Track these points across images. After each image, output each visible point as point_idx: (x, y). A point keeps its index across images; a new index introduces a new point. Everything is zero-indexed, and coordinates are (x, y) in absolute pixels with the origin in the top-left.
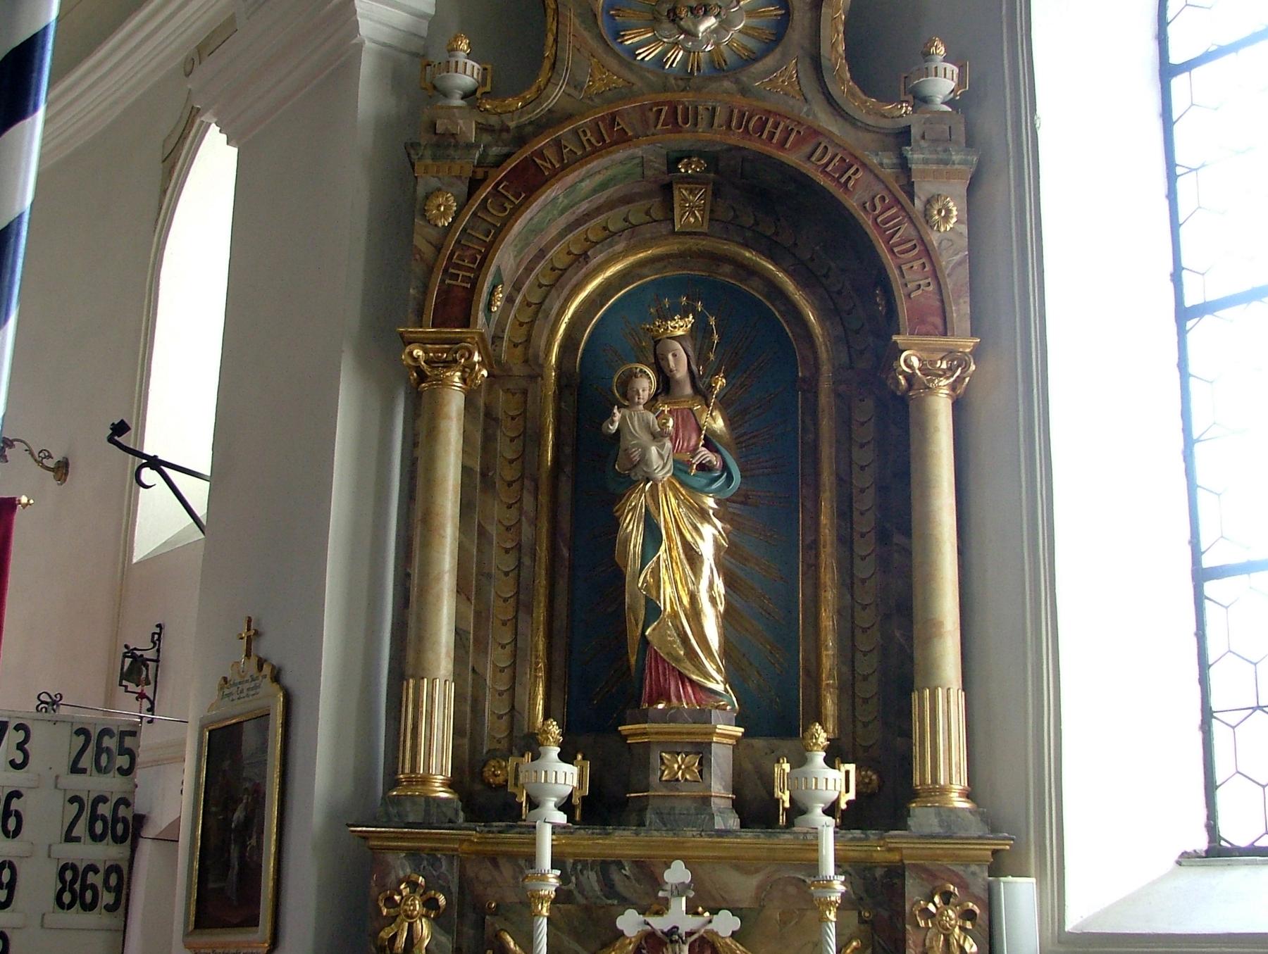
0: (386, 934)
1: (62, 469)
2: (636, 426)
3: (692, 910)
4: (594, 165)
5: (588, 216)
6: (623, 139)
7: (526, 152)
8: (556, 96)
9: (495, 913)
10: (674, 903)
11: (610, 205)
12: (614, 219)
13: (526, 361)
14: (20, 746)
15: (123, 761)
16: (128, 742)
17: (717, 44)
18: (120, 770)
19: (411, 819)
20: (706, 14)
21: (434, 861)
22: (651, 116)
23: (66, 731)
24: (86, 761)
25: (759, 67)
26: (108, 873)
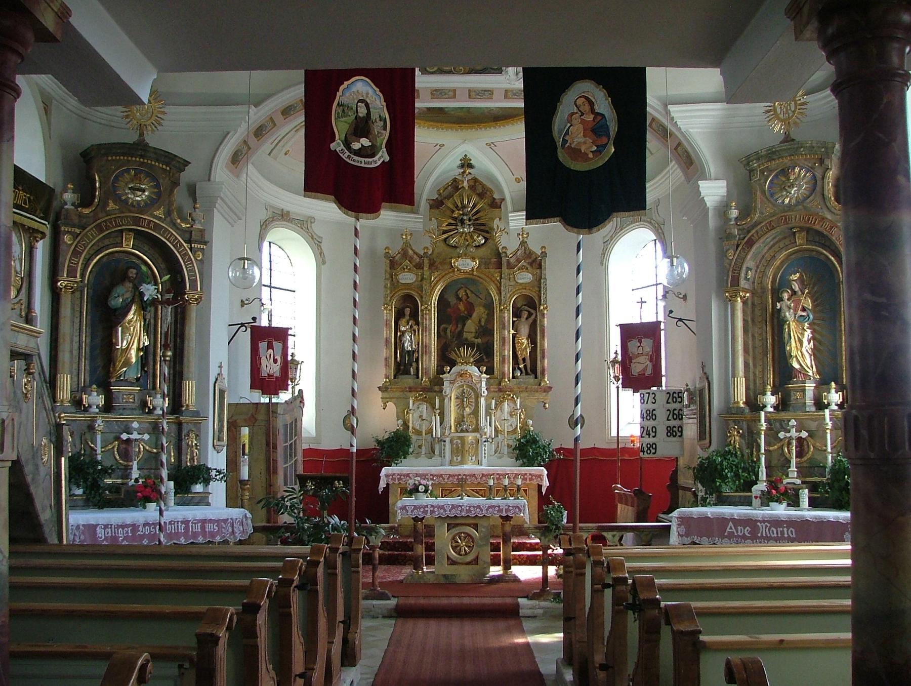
0: (728, 440)
1: (685, 298)
2: (784, 308)
3: (796, 431)
4: (767, 236)
5: (774, 245)
6: (773, 228)
7: (750, 234)
8: (756, 217)
9: (755, 434)
10: (791, 430)
11: (780, 241)
12: (782, 245)
13: (761, 289)
14: (654, 398)
15: (679, 400)
16: (680, 395)
17: (798, 195)
18: (679, 402)
19: (733, 412)
20: (793, 187)
21: (739, 422)
22: (780, 220)
23: (665, 394)
24: (670, 400)
25: (808, 200)
26: (678, 428)
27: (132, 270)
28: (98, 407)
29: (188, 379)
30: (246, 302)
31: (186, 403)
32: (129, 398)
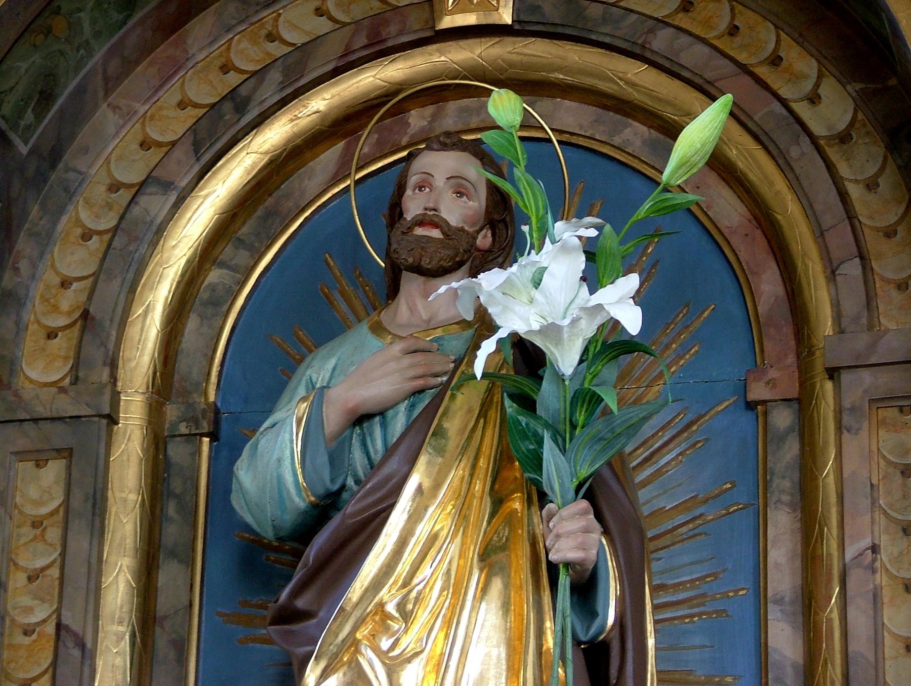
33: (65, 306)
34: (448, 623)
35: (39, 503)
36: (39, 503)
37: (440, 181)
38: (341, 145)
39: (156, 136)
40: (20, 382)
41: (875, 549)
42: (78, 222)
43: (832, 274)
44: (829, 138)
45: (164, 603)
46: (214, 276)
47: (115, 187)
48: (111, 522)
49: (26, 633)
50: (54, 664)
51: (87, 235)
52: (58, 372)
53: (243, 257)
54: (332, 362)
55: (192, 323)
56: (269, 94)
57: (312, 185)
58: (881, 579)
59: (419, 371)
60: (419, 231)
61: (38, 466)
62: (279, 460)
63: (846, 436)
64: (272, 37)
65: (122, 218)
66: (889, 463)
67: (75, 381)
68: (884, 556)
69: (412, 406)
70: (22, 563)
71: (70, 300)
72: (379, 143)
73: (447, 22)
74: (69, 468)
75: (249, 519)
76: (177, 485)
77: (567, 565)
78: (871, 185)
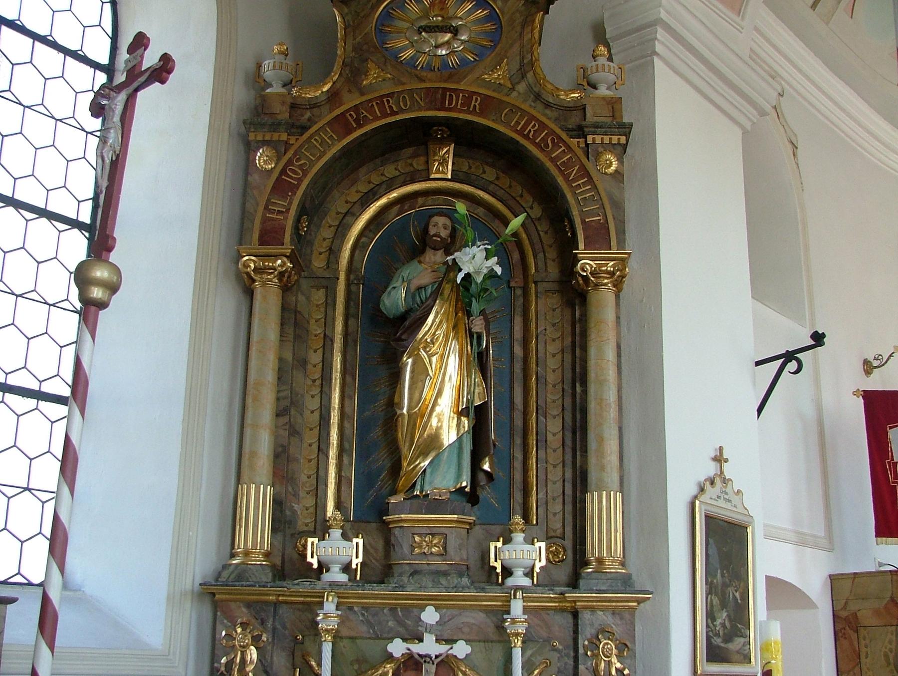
27: (436, 219)
28: (346, 568)
29: (600, 490)
30: (876, 363)
31: (593, 555)
32: (430, 545)
33: (324, 246)
34: (444, 346)
35: (318, 300)
36: (318, 300)
37: (440, 225)
38: (399, 206)
39: (349, 199)
40: (312, 267)
41: (545, 329)
42: (328, 223)
43: (535, 257)
44: (536, 219)
45: (350, 330)
46: (363, 239)
47: (338, 213)
48: (337, 306)
49: (316, 336)
50: (324, 345)
51: (330, 227)
52: (324, 264)
53: (371, 235)
54: (408, 271)
55: (357, 252)
56: (382, 190)
57: (391, 216)
58: (547, 337)
59: (435, 277)
60: (434, 238)
61: (317, 290)
62: (398, 299)
63: (539, 299)
64: (382, 175)
65: (341, 222)
66: (549, 307)
67: (328, 267)
68: (547, 332)
69: (432, 287)
70: (314, 317)
71: (326, 244)
72: (410, 206)
73: (433, 176)
74: (327, 291)
75: (385, 312)
76: (353, 297)
77: (477, 333)
78: (546, 233)
